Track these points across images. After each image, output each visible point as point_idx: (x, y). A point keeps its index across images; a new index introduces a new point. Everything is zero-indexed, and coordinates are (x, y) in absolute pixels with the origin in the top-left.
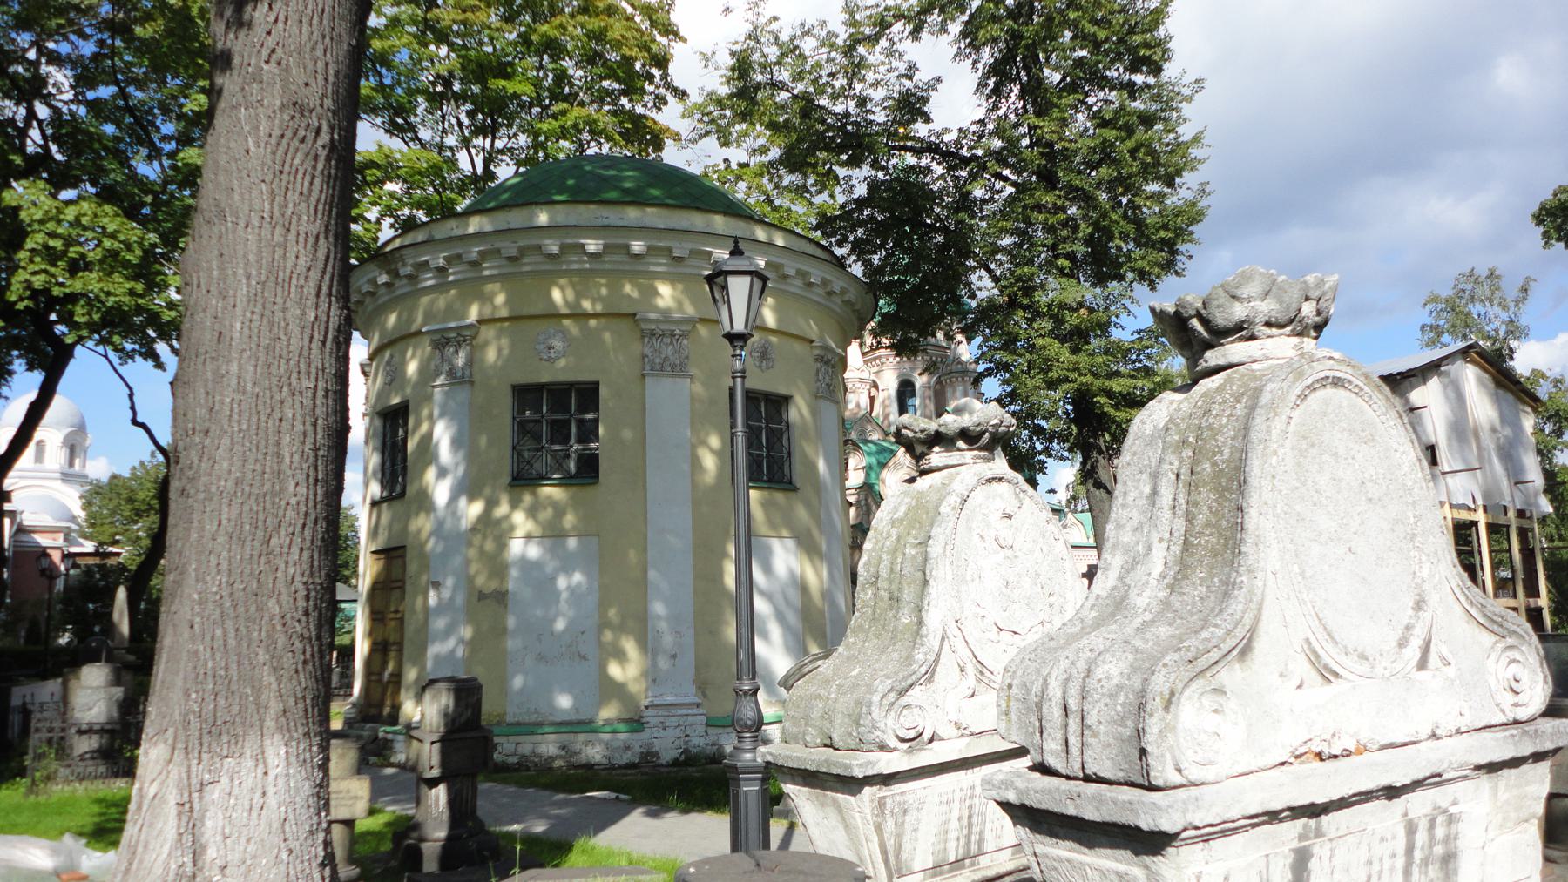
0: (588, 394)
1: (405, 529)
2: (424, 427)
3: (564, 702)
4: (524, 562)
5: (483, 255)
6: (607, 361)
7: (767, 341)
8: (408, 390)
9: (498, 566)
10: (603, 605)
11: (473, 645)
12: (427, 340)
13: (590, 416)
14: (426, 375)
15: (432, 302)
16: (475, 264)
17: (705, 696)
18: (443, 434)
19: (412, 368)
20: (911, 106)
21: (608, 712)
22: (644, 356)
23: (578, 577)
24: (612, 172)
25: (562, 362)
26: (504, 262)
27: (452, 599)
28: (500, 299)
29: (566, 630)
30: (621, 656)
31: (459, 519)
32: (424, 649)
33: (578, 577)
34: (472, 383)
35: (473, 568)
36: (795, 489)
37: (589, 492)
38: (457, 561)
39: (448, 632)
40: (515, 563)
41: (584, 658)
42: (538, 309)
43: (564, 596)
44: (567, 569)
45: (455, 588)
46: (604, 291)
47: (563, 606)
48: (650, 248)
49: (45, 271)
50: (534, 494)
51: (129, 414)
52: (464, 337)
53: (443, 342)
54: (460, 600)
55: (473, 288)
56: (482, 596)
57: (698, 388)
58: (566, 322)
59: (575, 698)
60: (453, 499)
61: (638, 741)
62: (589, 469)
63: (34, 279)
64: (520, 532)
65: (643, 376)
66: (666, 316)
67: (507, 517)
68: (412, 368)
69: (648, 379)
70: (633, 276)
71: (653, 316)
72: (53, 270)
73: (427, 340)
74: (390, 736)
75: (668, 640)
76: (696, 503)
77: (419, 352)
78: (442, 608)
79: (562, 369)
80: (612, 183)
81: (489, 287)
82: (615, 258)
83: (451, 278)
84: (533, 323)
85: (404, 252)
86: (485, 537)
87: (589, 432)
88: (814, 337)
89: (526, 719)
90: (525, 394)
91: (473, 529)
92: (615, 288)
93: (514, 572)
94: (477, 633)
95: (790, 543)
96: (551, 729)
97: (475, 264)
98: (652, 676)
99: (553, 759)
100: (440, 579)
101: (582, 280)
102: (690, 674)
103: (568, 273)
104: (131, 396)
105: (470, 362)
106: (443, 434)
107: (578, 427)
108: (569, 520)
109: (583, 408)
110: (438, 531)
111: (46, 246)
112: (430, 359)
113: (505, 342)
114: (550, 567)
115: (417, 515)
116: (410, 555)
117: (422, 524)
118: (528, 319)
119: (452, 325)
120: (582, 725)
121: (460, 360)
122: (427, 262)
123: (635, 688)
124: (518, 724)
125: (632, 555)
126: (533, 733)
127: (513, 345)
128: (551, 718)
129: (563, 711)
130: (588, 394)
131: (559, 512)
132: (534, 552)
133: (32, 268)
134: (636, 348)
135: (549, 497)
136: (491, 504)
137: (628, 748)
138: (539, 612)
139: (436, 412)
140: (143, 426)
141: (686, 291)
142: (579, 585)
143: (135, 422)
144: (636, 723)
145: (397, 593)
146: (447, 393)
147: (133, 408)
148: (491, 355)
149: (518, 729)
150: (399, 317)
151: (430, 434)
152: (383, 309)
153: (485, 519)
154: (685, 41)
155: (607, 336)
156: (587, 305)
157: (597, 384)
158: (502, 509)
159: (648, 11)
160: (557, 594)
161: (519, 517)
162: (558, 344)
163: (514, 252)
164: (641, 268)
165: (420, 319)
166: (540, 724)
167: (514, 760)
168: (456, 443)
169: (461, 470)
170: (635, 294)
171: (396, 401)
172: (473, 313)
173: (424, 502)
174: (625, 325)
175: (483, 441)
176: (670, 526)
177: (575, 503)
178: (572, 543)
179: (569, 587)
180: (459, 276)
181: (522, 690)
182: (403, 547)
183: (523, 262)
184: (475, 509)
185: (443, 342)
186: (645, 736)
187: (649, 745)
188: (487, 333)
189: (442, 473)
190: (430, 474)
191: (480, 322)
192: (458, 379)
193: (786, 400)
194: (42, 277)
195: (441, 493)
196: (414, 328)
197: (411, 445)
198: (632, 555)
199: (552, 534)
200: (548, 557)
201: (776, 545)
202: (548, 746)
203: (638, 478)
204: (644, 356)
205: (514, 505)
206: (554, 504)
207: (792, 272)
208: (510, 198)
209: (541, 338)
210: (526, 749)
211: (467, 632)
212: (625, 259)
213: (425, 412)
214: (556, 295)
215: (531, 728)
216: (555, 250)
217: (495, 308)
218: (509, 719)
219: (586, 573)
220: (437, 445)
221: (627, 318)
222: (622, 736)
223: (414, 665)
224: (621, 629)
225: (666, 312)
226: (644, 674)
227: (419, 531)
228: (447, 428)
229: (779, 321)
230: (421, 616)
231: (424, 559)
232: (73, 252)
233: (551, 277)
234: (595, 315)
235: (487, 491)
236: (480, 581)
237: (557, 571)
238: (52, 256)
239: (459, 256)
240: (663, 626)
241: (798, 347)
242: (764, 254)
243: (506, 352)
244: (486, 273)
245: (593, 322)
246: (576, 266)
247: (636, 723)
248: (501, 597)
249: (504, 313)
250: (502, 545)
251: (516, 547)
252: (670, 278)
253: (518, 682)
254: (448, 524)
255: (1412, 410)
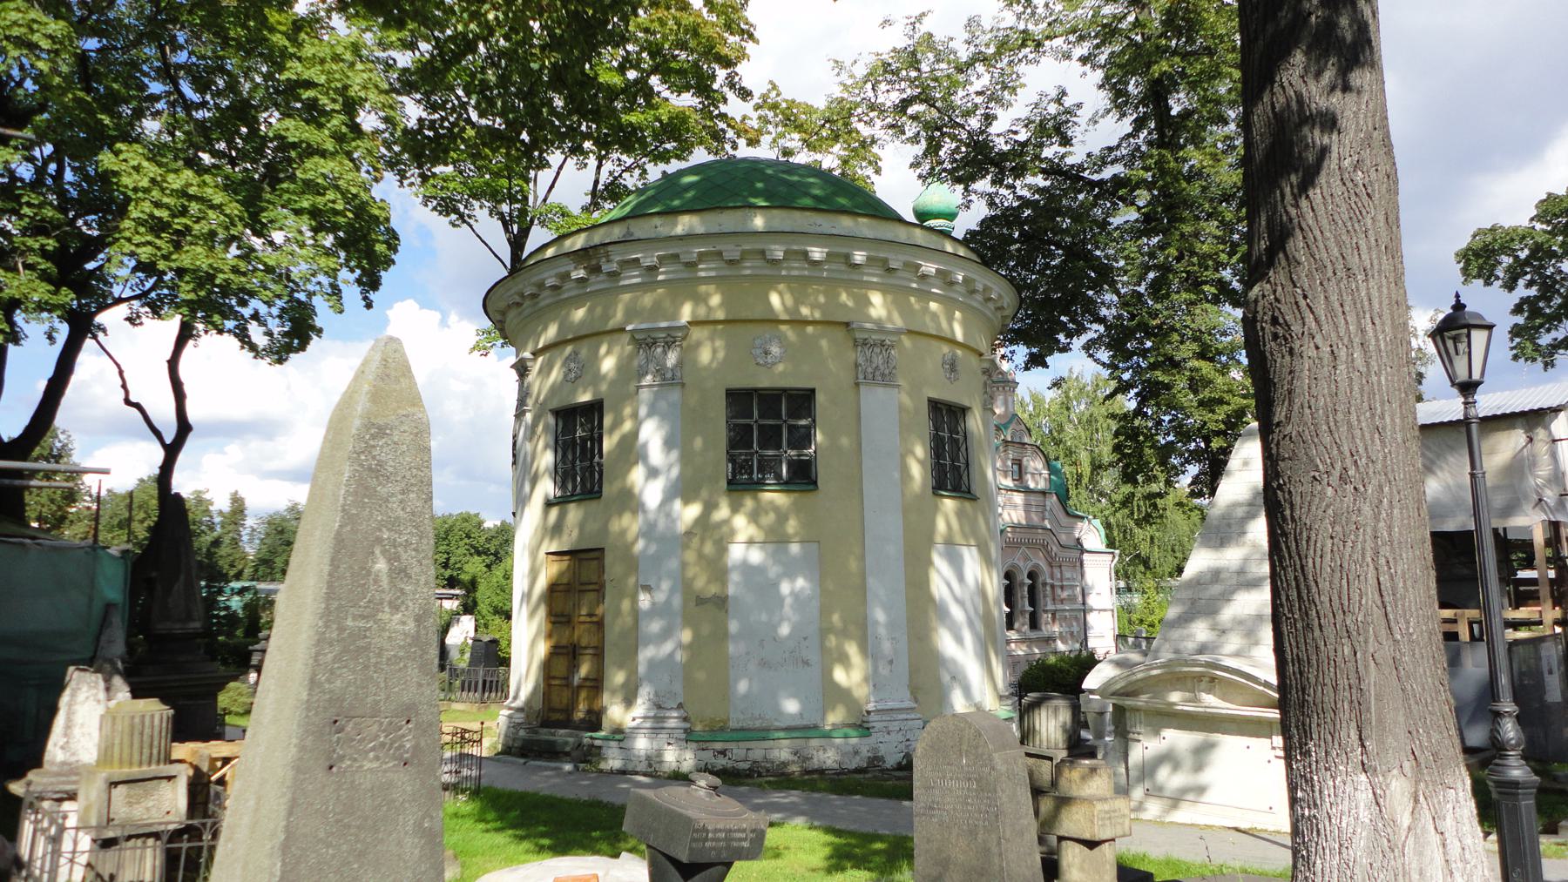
0: (803, 401)
1: (605, 529)
2: (627, 426)
3: (791, 706)
4: (746, 568)
5: (702, 257)
6: (821, 367)
7: (954, 355)
8: (604, 387)
9: (718, 569)
10: (825, 611)
11: (692, 648)
12: (626, 338)
13: (803, 422)
14: (628, 374)
15: (634, 301)
16: (691, 265)
17: (916, 700)
18: (652, 434)
19: (608, 364)
20: (1056, 128)
21: (835, 717)
22: (857, 365)
23: (800, 583)
24: (796, 178)
25: (780, 367)
26: (723, 265)
27: (668, 602)
28: (715, 300)
29: (790, 636)
30: (844, 660)
31: (674, 521)
32: (635, 651)
33: (800, 583)
34: (683, 385)
35: (690, 572)
36: (974, 499)
37: (808, 499)
38: (673, 564)
39: (666, 634)
40: (735, 567)
41: (806, 663)
42: (758, 314)
43: (788, 601)
44: (791, 576)
45: (672, 591)
46: (822, 299)
47: (787, 609)
48: (868, 258)
49: (149, 243)
50: (756, 499)
51: (122, 395)
52: (672, 337)
53: (646, 342)
54: (677, 601)
55: (686, 287)
56: (701, 601)
57: (906, 400)
58: (783, 328)
59: (801, 702)
60: (668, 498)
61: (865, 746)
62: (803, 477)
63: (139, 251)
64: (741, 537)
65: (857, 385)
66: (880, 327)
67: (727, 522)
68: (608, 364)
69: (862, 388)
70: (849, 284)
71: (868, 325)
72: (158, 242)
73: (626, 338)
74: (597, 743)
75: (887, 646)
76: (906, 511)
77: (617, 349)
78: (655, 611)
79: (779, 374)
80: (802, 189)
81: (703, 288)
82: (834, 267)
83: (660, 278)
84: (750, 326)
85: (610, 248)
86: (702, 541)
87: (802, 438)
88: (983, 350)
89: (750, 724)
90: (739, 399)
91: (689, 533)
92: (832, 297)
93: (735, 577)
94: (696, 636)
95: (974, 550)
96: (781, 734)
97: (691, 265)
98: (873, 680)
99: (785, 764)
100: (652, 583)
101: (799, 287)
102: (905, 680)
103: (788, 279)
104: (121, 373)
105: (680, 364)
106: (652, 434)
107: (790, 432)
108: (792, 526)
109: (795, 413)
110: (649, 532)
111: (152, 216)
112: (631, 357)
113: (719, 343)
114: (773, 571)
115: (620, 515)
116: (608, 559)
117: (630, 524)
118: (744, 323)
119: (664, 324)
120: (805, 730)
121: (672, 359)
122: (637, 260)
123: (861, 692)
124: (742, 729)
125: (853, 565)
126: (764, 739)
127: (728, 347)
128: (777, 724)
129: (791, 715)
130: (803, 401)
131: (782, 517)
132: (756, 556)
133: (137, 239)
134: (851, 355)
135: (771, 502)
136: (710, 507)
137: (856, 753)
138: (764, 617)
139: (643, 411)
140: (138, 406)
141: (894, 302)
142: (802, 589)
143: (128, 402)
144: (862, 726)
145: (591, 596)
146: (656, 393)
147: (124, 386)
148: (705, 356)
149: (749, 735)
150: (590, 311)
151: (635, 434)
152: (577, 301)
153: (703, 522)
154: (757, 42)
155: (824, 343)
156: (805, 311)
157: (813, 391)
158: (723, 512)
159: (722, 11)
160: (781, 600)
161: (740, 521)
162: (775, 350)
163: (736, 255)
164: (856, 277)
165: (619, 315)
166: (768, 730)
167: (746, 766)
168: (668, 444)
169: (675, 472)
170: (850, 304)
171: (585, 397)
172: (686, 313)
173: (630, 501)
174: (840, 333)
175: (698, 443)
176: (885, 529)
177: (797, 508)
178: (795, 548)
179: (792, 593)
180: (671, 276)
181: (746, 697)
182: (602, 550)
183: (744, 265)
184: (689, 513)
185: (646, 342)
186: (872, 740)
187: (875, 749)
188: (697, 334)
189: (653, 473)
190: (637, 475)
191: (694, 323)
192: (670, 380)
193: (964, 410)
194: (149, 249)
195: (652, 494)
196: (611, 324)
197: (607, 444)
198: (853, 565)
199: (775, 539)
200: (770, 562)
201: (965, 551)
202: (782, 752)
203: (855, 485)
204: (857, 365)
205: (735, 509)
206: (776, 509)
207: (980, 287)
208: (694, 198)
209: (758, 342)
210: (757, 754)
211: (686, 636)
212: (843, 268)
213: (628, 411)
214: (775, 299)
215: (763, 734)
216: (780, 255)
217: (710, 309)
218: (732, 724)
219: (805, 578)
220: (645, 445)
221: (845, 326)
222: (854, 741)
223: (621, 667)
224: (844, 634)
225: (878, 322)
226: (866, 679)
227: (623, 532)
228: (659, 428)
229: (965, 335)
230: (629, 620)
231: (632, 563)
232: (179, 222)
233: (772, 282)
234: (814, 323)
235: (704, 493)
236: (700, 583)
237: (780, 577)
238: (157, 227)
239: (676, 257)
240: (882, 631)
241: (974, 359)
242: (963, 269)
243: (721, 355)
244: (702, 274)
245: (810, 329)
246: (795, 273)
247: (862, 726)
248: (721, 602)
249: (720, 315)
250: (722, 547)
251: (736, 552)
252: (883, 289)
253: (743, 686)
254: (662, 524)
255: (1554, 441)
